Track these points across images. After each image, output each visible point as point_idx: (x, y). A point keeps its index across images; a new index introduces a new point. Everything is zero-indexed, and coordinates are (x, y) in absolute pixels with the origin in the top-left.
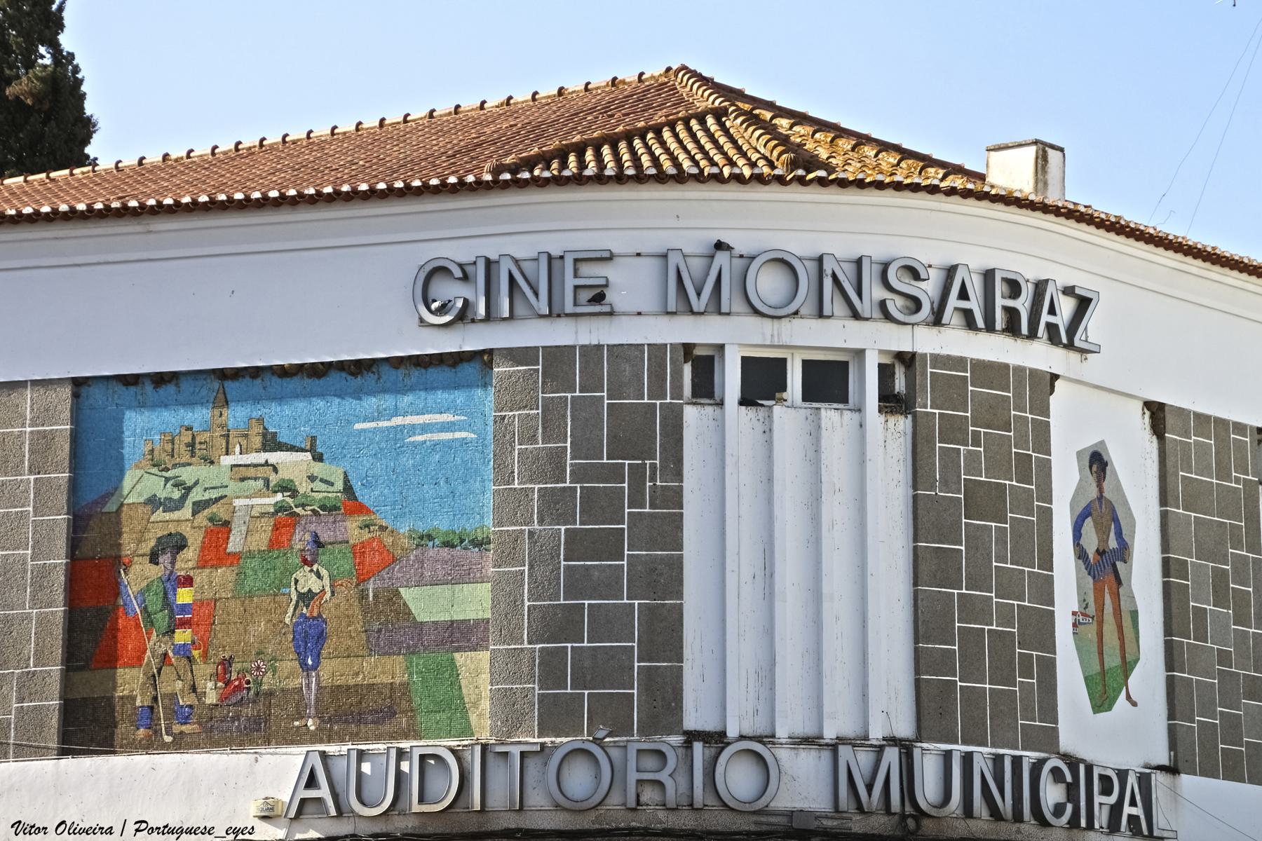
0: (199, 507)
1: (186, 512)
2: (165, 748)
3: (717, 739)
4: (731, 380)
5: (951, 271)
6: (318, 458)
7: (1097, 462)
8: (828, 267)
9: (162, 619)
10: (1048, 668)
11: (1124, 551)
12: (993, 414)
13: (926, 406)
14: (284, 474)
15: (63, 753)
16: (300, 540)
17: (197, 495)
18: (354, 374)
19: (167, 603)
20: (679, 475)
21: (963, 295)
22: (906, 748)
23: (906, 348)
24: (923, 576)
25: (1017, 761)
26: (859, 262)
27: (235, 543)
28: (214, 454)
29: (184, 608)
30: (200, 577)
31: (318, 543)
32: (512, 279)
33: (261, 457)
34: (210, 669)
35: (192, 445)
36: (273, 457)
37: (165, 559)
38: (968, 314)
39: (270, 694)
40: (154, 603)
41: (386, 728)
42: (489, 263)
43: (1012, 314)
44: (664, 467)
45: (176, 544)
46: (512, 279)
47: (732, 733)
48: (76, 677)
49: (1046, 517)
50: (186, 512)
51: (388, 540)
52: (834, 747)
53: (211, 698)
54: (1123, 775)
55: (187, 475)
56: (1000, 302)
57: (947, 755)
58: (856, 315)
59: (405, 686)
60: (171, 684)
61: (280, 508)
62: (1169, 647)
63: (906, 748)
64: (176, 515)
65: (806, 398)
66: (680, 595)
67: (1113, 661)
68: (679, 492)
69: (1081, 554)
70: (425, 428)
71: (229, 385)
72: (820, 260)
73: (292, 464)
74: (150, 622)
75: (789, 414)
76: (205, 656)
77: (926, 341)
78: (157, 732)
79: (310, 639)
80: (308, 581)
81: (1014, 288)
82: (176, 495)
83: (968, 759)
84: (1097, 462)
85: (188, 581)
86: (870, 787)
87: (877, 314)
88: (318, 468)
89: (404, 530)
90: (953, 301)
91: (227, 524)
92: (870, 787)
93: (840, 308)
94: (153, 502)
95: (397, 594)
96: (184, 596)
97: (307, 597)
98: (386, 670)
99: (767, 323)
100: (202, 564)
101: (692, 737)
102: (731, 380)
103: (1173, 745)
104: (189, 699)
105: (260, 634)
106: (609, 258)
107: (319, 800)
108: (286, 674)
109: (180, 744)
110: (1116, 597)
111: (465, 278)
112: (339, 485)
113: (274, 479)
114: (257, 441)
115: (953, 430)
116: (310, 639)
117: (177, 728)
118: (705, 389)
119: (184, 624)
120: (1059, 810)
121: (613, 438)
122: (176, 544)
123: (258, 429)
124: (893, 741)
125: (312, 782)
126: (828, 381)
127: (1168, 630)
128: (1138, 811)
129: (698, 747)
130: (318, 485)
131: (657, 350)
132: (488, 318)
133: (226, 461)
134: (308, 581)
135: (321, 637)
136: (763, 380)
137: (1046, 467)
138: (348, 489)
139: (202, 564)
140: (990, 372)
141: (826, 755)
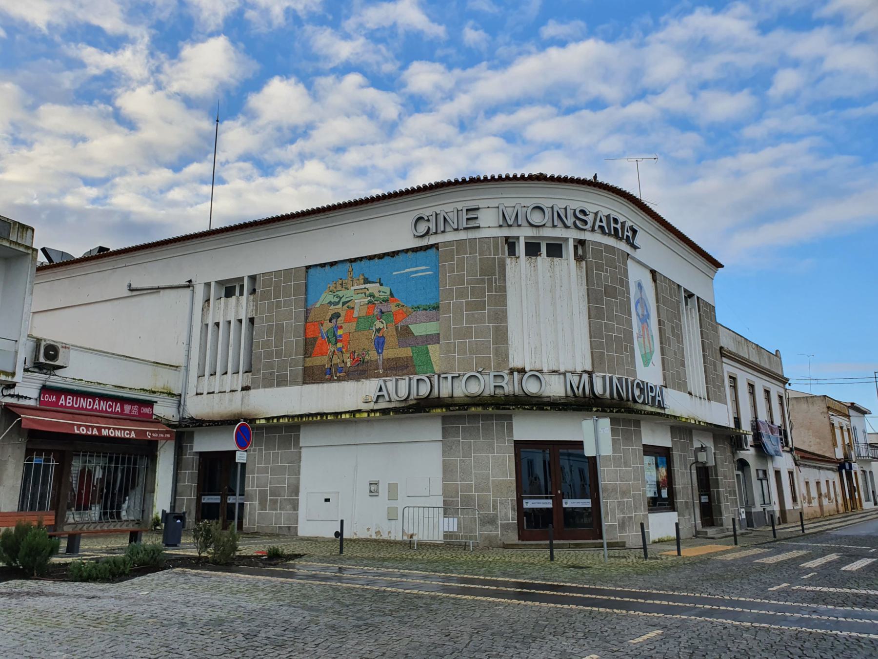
0: (344, 304)
1: (340, 305)
2: (334, 381)
3: (522, 371)
4: (521, 249)
5: (596, 214)
6: (381, 285)
7: (640, 286)
8: (555, 209)
9: (333, 340)
10: (632, 349)
11: (648, 316)
12: (611, 263)
13: (590, 257)
14: (370, 291)
15: (304, 383)
16: (376, 312)
17: (343, 300)
18: (393, 257)
19: (335, 335)
20: (505, 281)
21: (601, 221)
22: (590, 374)
23: (583, 238)
24: (592, 316)
25: (627, 380)
26: (566, 209)
27: (356, 314)
28: (349, 286)
29: (340, 336)
30: (344, 326)
31: (382, 313)
32: (445, 218)
33: (363, 286)
34: (348, 355)
35: (342, 284)
36: (367, 286)
37: (334, 321)
38: (601, 227)
39: (368, 362)
40: (331, 335)
41: (405, 371)
42: (437, 214)
43: (616, 229)
44: (499, 279)
45: (337, 316)
46: (445, 218)
47: (527, 369)
48: (307, 359)
49: (629, 299)
50: (340, 305)
51: (405, 310)
52: (564, 374)
53: (349, 364)
54: (656, 386)
55: (340, 294)
56: (613, 225)
57: (604, 378)
58: (566, 227)
59: (412, 357)
60: (336, 360)
61: (370, 302)
62: (662, 348)
63: (590, 374)
64: (337, 307)
65: (548, 256)
66: (506, 322)
67: (648, 351)
68: (505, 287)
69: (638, 315)
70: (416, 272)
71: (353, 264)
72: (552, 208)
73: (373, 288)
74: (329, 341)
75: (543, 260)
76: (347, 351)
77: (587, 236)
78: (332, 376)
79: (380, 344)
80: (378, 325)
81: (616, 221)
82: (337, 300)
83: (611, 379)
84: (640, 286)
85: (341, 327)
86: (578, 388)
87: (573, 226)
88: (382, 288)
89: (410, 305)
90: (598, 223)
91: (353, 308)
92: (578, 388)
93: (560, 225)
94: (330, 303)
95: (408, 326)
96: (340, 332)
97: (379, 330)
98: (405, 352)
99: (534, 229)
100: (346, 321)
101: (512, 371)
102: (521, 249)
103: (665, 379)
104: (343, 365)
105: (364, 343)
106: (478, 209)
107: (383, 396)
108: (373, 355)
109: (339, 380)
110: (647, 330)
111: (428, 220)
112: (388, 293)
113: (368, 293)
114: (362, 281)
115: (599, 267)
116: (380, 344)
117: (338, 374)
118: (512, 252)
119: (341, 341)
120: (639, 397)
121: (481, 269)
122: (337, 316)
123: (361, 277)
124: (585, 372)
125: (381, 390)
126: (555, 250)
127: (661, 343)
128: (660, 399)
129: (516, 373)
130: (381, 294)
131: (496, 238)
132: (436, 233)
133: (352, 288)
134: (378, 325)
135: (383, 343)
136: (532, 249)
137: (628, 283)
138: (391, 294)
139: (346, 321)
140: (610, 249)
141: (562, 377)
